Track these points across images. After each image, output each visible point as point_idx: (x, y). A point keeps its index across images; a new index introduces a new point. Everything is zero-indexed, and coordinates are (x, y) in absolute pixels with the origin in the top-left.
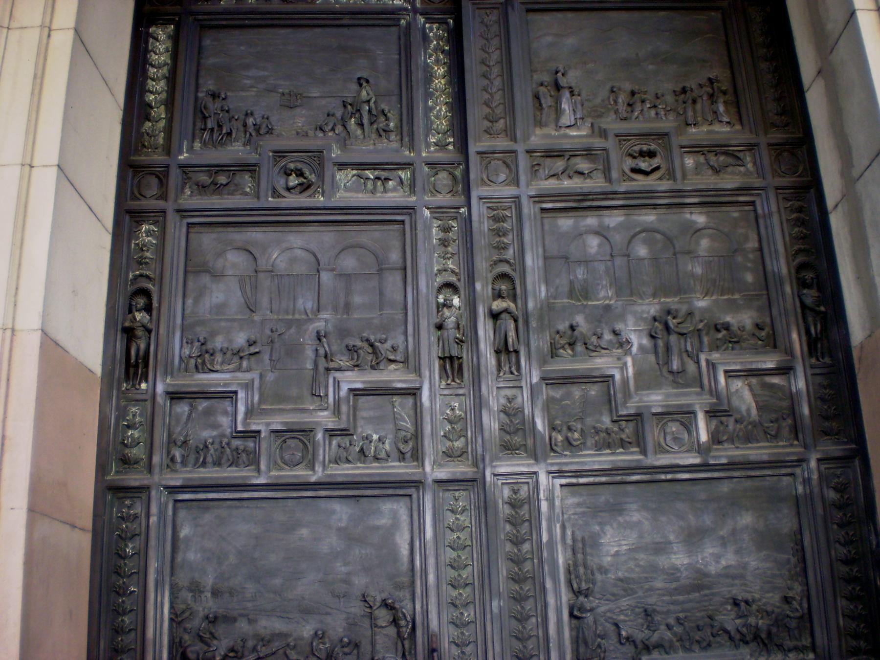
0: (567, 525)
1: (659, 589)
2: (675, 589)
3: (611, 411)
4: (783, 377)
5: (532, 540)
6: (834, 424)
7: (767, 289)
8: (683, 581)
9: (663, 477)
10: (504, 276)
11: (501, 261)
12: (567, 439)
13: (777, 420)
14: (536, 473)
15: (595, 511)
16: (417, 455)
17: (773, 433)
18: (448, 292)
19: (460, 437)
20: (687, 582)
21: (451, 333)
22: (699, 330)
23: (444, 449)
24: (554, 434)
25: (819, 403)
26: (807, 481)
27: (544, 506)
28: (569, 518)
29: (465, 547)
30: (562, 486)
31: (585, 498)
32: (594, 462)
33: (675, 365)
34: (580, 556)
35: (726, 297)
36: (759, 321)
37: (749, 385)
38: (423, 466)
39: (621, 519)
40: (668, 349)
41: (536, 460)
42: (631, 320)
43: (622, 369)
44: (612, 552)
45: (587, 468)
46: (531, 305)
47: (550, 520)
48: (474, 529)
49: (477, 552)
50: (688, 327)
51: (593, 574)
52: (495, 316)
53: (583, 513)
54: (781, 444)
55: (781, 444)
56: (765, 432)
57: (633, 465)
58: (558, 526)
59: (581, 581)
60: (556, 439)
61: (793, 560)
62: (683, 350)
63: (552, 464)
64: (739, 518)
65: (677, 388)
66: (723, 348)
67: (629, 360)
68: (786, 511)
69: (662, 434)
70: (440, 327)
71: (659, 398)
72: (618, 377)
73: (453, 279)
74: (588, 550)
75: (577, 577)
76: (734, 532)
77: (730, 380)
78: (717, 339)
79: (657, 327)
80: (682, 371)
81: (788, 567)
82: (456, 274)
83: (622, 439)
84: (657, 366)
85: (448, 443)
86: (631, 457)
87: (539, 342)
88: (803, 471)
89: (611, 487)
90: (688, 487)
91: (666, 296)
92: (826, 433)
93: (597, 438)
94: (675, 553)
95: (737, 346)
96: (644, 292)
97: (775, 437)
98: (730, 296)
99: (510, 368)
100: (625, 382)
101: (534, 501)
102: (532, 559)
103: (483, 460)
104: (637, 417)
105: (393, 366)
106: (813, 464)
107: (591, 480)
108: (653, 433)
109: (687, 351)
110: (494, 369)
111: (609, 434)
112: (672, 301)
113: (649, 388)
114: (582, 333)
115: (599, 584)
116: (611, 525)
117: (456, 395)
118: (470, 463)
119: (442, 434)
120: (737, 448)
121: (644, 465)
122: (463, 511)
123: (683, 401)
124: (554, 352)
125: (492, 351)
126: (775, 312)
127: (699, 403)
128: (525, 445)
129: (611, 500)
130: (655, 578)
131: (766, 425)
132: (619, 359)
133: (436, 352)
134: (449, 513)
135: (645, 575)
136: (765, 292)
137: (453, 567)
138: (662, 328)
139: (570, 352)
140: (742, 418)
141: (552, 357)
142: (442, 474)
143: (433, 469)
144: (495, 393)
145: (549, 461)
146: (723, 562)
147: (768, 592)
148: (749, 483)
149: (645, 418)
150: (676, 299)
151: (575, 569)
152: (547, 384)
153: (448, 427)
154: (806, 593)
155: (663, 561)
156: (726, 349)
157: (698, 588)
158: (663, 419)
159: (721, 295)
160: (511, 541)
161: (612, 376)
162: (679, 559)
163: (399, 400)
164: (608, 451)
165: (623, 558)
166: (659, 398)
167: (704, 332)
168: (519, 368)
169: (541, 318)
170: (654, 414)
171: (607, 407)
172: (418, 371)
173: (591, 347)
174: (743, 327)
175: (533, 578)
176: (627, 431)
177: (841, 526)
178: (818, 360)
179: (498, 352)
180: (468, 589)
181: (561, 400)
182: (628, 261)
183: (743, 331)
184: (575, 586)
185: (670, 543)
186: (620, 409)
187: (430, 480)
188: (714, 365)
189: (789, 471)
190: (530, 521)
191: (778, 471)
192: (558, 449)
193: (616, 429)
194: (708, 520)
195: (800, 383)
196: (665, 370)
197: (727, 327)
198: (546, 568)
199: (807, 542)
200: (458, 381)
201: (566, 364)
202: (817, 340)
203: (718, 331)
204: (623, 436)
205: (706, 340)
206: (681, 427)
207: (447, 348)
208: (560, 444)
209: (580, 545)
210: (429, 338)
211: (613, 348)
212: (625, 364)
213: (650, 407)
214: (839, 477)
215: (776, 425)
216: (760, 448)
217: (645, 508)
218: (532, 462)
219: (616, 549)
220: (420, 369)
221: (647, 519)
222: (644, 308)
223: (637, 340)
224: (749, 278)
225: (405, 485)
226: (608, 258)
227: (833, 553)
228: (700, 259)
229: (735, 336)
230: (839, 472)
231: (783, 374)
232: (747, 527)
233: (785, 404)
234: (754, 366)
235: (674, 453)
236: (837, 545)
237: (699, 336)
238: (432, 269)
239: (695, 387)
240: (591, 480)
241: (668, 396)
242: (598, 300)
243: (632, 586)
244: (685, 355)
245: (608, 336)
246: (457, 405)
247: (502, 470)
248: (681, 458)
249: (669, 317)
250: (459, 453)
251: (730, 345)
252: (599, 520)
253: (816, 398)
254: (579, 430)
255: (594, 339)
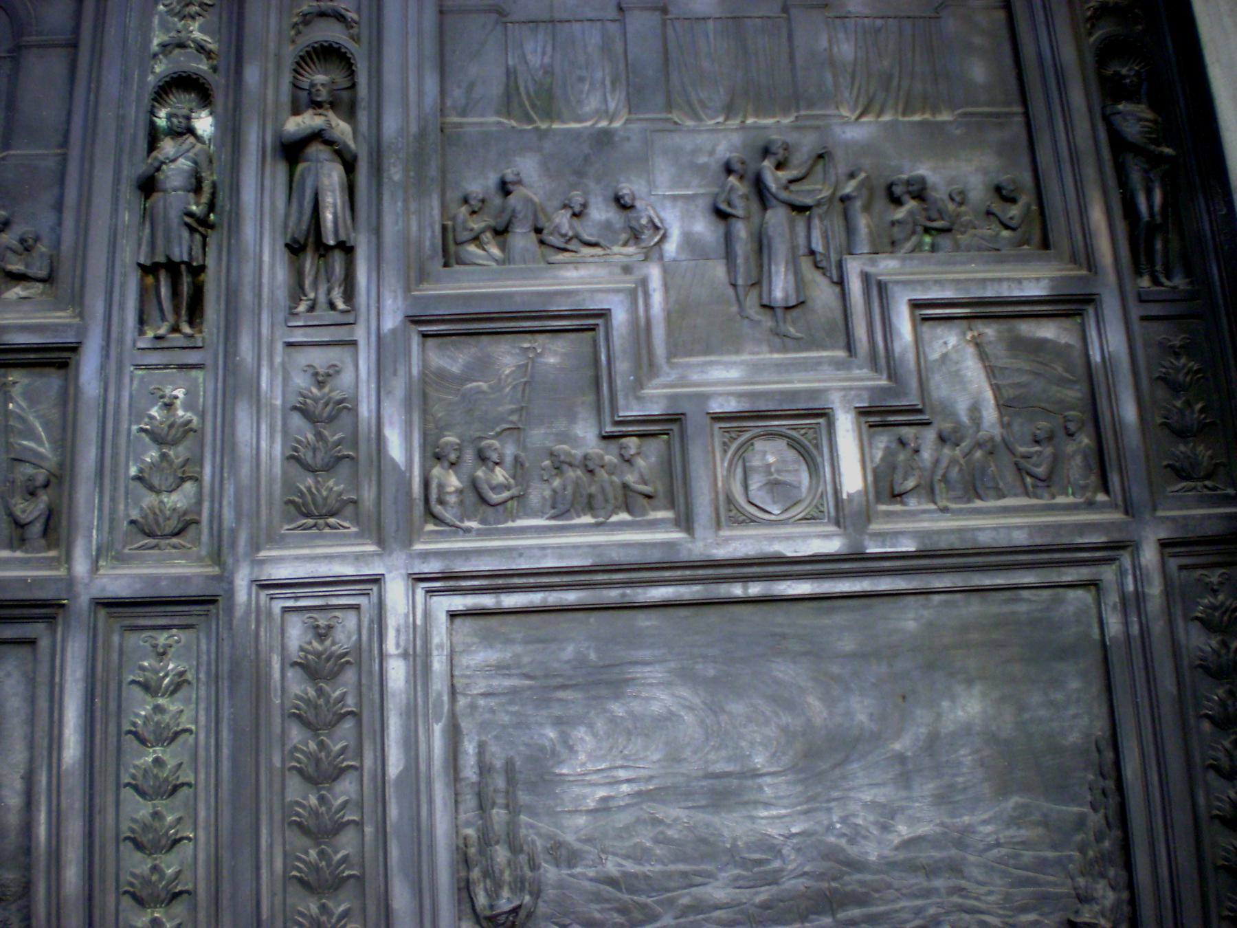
0: (465, 724)
1: (717, 908)
2: (765, 906)
3: (599, 410)
4: (1067, 323)
5: (360, 769)
6: (1201, 448)
7: (1024, 102)
8: (790, 884)
9: (737, 590)
10: (329, 54)
11: (322, 14)
12: (474, 485)
13: (1051, 438)
14: (377, 580)
15: (544, 688)
16: (54, 530)
17: (1041, 471)
18: (181, 102)
19: (183, 480)
20: (800, 884)
21: (176, 200)
22: (845, 199)
23: (135, 514)
24: (437, 471)
25: (1161, 392)
26: (1133, 603)
27: (397, 673)
28: (473, 707)
29: (176, 788)
30: (453, 615)
31: (519, 649)
32: (543, 548)
33: (780, 288)
34: (499, 815)
35: (917, 118)
36: (1004, 178)
37: (978, 344)
38: (69, 558)
39: (618, 709)
40: (761, 245)
41: (380, 542)
42: (663, 173)
43: (632, 294)
44: (591, 804)
45: (524, 564)
46: (391, 124)
47: (411, 713)
48: (202, 736)
49: (207, 801)
50: (815, 190)
51: (534, 866)
52: (292, 151)
53: (513, 692)
54: (1061, 500)
55: (1061, 500)
56: (1019, 469)
57: (655, 556)
58: (438, 729)
59: (498, 885)
60: (441, 486)
61: (1095, 820)
62: (802, 250)
63: (425, 556)
64: (945, 704)
65: (785, 349)
66: (909, 245)
67: (654, 273)
68: (1075, 684)
69: (739, 470)
70: (148, 186)
71: (734, 374)
72: (620, 317)
73: (202, 66)
74: (523, 797)
75: (487, 874)
76: (932, 743)
77: (926, 328)
78: (893, 223)
79: (732, 189)
80: (798, 305)
81: (1079, 837)
82: (209, 54)
83: (625, 486)
84: (730, 292)
85: (149, 500)
86: (652, 535)
87: (406, 220)
88: (1122, 573)
89: (593, 618)
90: (804, 618)
91: (758, 113)
92: (1180, 473)
93: (557, 483)
94: (767, 805)
95: (945, 241)
96: (702, 102)
97: (1047, 482)
98: (927, 116)
99: (329, 292)
100: (641, 332)
101: (371, 658)
102: (359, 825)
103: (233, 545)
104: (670, 425)
105: (18, 291)
106: (1149, 555)
107: (536, 598)
108: (710, 470)
109: (812, 253)
110: (282, 295)
111: (591, 472)
112: (775, 125)
113: (707, 351)
114: (528, 200)
115: (550, 893)
116: (591, 726)
117: (181, 367)
118: (204, 553)
119: (133, 471)
120: (945, 510)
121: (684, 556)
122: (176, 687)
123: (799, 382)
124: (450, 252)
125: (280, 246)
126: (1045, 157)
127: (841, 387)
128: (355, 502)
129: (593, 656)
130: (711, 875)
131: (1022, 449)
132: (627, 269)
133: (131, 253)
134: (137, 692)
135: (682, 867)
136: (1018, 109)
137: (139, 846)
138: (750, 192)
139: (495, 251)
140: (958, 428)
141: (446, 265)
142: (119, 581)
143: (95, 568)
144: (278, 360)
145: (418, 547)
146: (904, 830)
147: (1024, 909)
148: (974, 608)
149: (690, 430)
150: (786, 121)
151: (481, 852)
152: (425, 336)
153: (152, 455)
154: (1126, 909)
155: (732, 826)
156: (918, 247)
157: (828, 902)
158: (742, 431)
159: (904, 114)
160: (300, 771)
161: (604, 314)
162: (775, 818)
163: (26, 381)
164: (587, 519)
165: (622, 819)
166: (734, 374)
167: (858, 204)
168: (349, 294)
169: (418, 160)
170: (717, 418)
171: (590, 398)
172: (77, 300)
173: (553, 240)
174: (962, 192)
175: (360, 879)
176: (640, 462)
177: (1222, 723)
178: (1156, 281)
179: (295, 249)
180: (179, 908)
181: (464, 379)
182: (664, 24)
183: (961, 204)
184: (482, 900)
185: (755, 774)
186: (621, 401)
187: (84, 600)
188: (882, 287)
189: (1084, 573)
190: (356, 715)
191: (1053, 576)
192: (448, 515)
193: (611, 458)
194: (861, 710)
195: (1110, 339)
196: (751, 301)
197: (920, 191)
198: (394, 852)
199: (1131, 770)
200: (186, 329)
201: (485, 279)
202: (1153, 229)
203: (897, 201)
204: (630, 478)
205: (863, 223)
206: (791, 454)
207: (160, 242)
208: (452, 499)
209: (501, 783)
210: (115, 211)
211: (614, 243)
212: (644, 282)
213: (705, 397)
214: (1215, 592)
215: (1049, 450)
216: (1006, 511)
217: (686, 676)
218: (372, 548)
219: (602, 793)
220: (82, 296)
221: (691, 708)
222: (702, 139)
223: (682, 223)
224: (978, 72)
225: (17, 612)
226: (612, 13)
227: (1201, 800)
228: (850, 23)
229: (941, 214)
230: (1214, 577)
231: (1066, 315)
232: (966, 729)
233: (1074, 394)
234: (990, 292)
235: (771, 523)
236: (1212, 776)
237: (846, 216)
238: (147, 41)
239: (833, 347)
240: (536, 598)
241: (757, 368)
242: (579, 119)
243: (643, 899)
244: (806, 264)
245: (601, 212)
246: (180, 393)
247: (283, 572)
248: (788, 538)
249: (767, 164)
250: (172, 525)
251: (928, 239)
252: (557, 711)
253: (1154, 381)
254: (509, 460)
255: (563, 220)
